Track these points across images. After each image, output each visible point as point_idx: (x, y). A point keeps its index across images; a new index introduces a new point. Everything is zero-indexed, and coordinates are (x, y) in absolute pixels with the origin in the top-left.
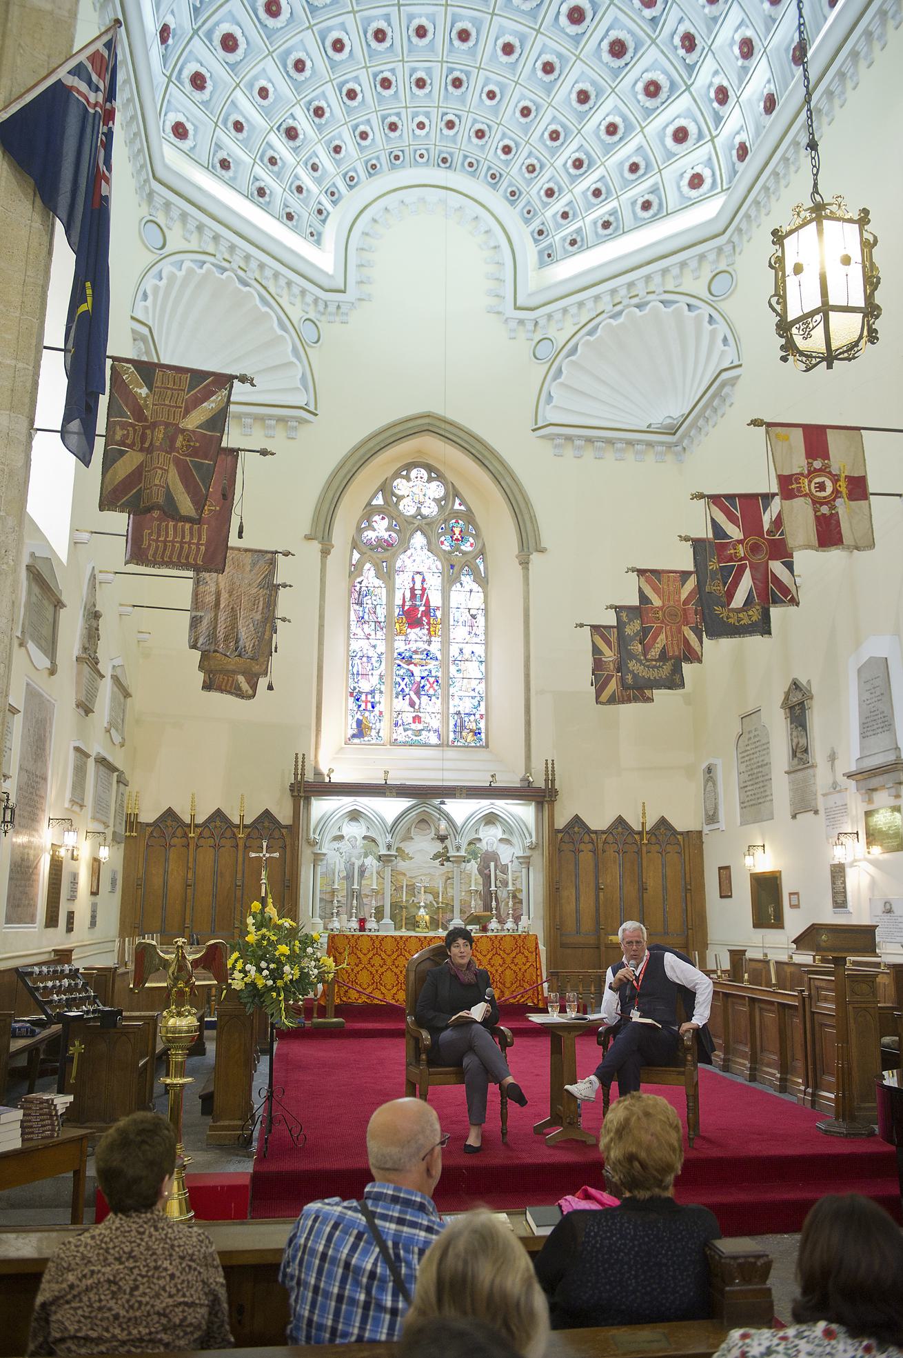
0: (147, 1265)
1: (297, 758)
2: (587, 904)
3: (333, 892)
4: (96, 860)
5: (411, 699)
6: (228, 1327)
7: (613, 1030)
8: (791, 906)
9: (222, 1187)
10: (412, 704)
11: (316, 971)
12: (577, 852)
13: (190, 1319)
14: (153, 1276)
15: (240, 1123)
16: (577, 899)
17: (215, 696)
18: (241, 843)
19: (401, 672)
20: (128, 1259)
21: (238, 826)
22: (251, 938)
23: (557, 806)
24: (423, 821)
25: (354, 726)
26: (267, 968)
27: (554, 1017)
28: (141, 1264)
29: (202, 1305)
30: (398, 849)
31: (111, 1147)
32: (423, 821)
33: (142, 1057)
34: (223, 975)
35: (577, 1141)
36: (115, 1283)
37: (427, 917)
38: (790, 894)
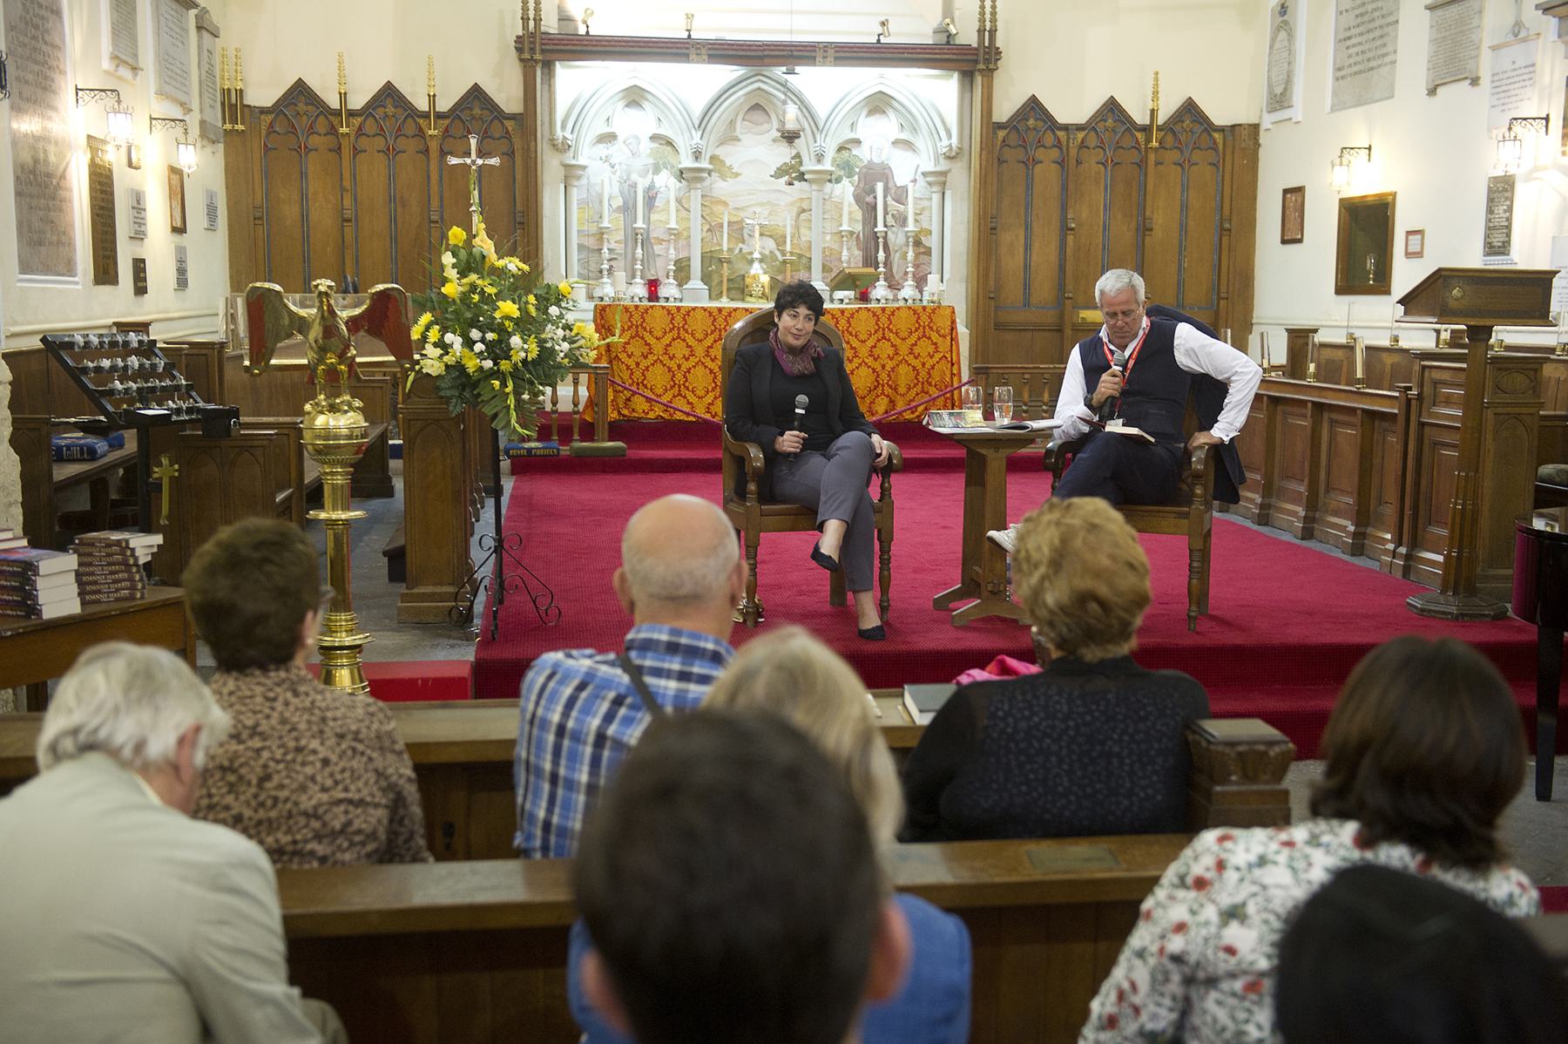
0: (283, 746)
2: (1045, 254)
3: (601, 234)
4: (175, 171)
6: (422, 842)
7: (1074, 445)
8: (1408, 255)
9: (425, 680)
11: (566, 346)
12: (1030, 163)
13: (357, 824)
14: (294, 761)
15: (451, 589)
16: (1028, 248)
18: (434, 146)
20: (251, 737)
21: (426, 115)
22: (452, 289)
23: (999, 79)
24: (757, 107)
26: (483, 340)
27: (972, 421)
28: (274, 744)
29: (376, 806)
30: (713, 159)
31: (212, 570)
32: (757, 108)
33: (282, 489)
34: (404, 348)
35: (1003, 620)
36: (234, 771)
37: (765, 279)
38: (1409, 233)
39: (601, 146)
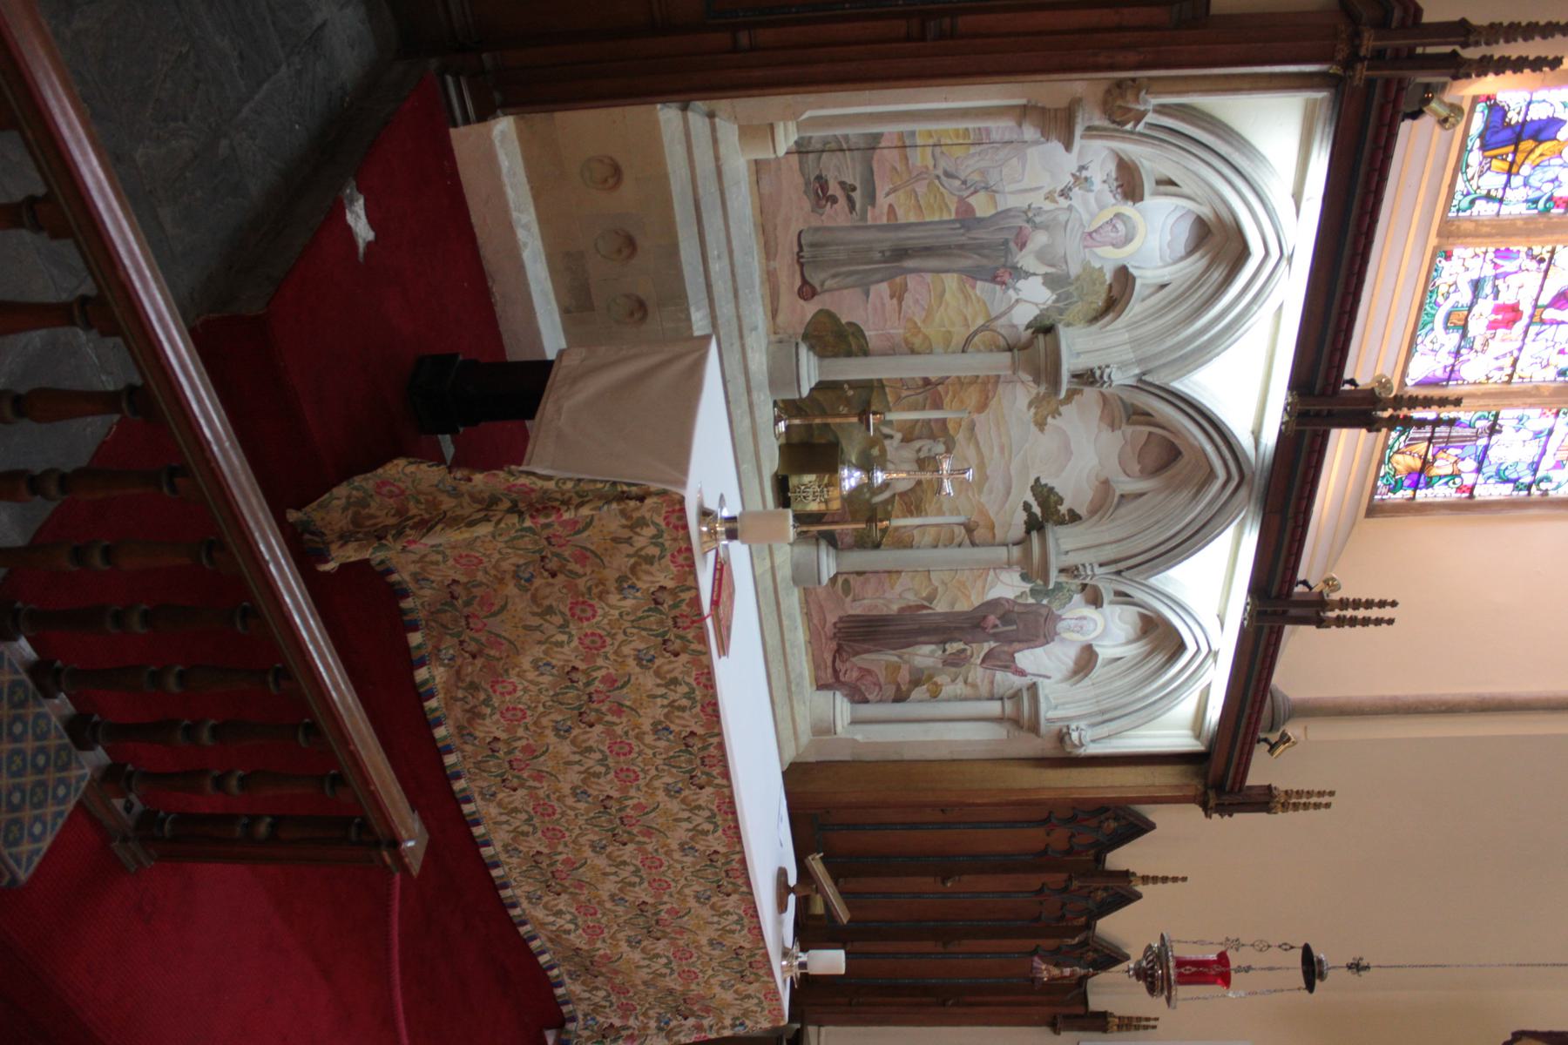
25: (1538, 113)
39: (1111, 167)
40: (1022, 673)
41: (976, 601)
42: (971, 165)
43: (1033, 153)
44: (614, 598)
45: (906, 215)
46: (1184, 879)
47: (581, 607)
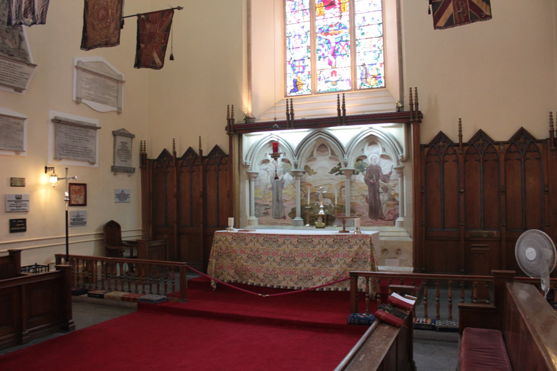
1: (228, 108)
5: (329, 60)
10: (330, 63)
17: (143, 70)
19: (322, 42)
25: (292, 84)
39: (264, 165)
40: (391, 173)
41: (365, 185)
42: (263, 188)
43: (261, 178)
44: (233, 246)
45: (271, 199)
46: (460, 119)
47: (235, 251)
